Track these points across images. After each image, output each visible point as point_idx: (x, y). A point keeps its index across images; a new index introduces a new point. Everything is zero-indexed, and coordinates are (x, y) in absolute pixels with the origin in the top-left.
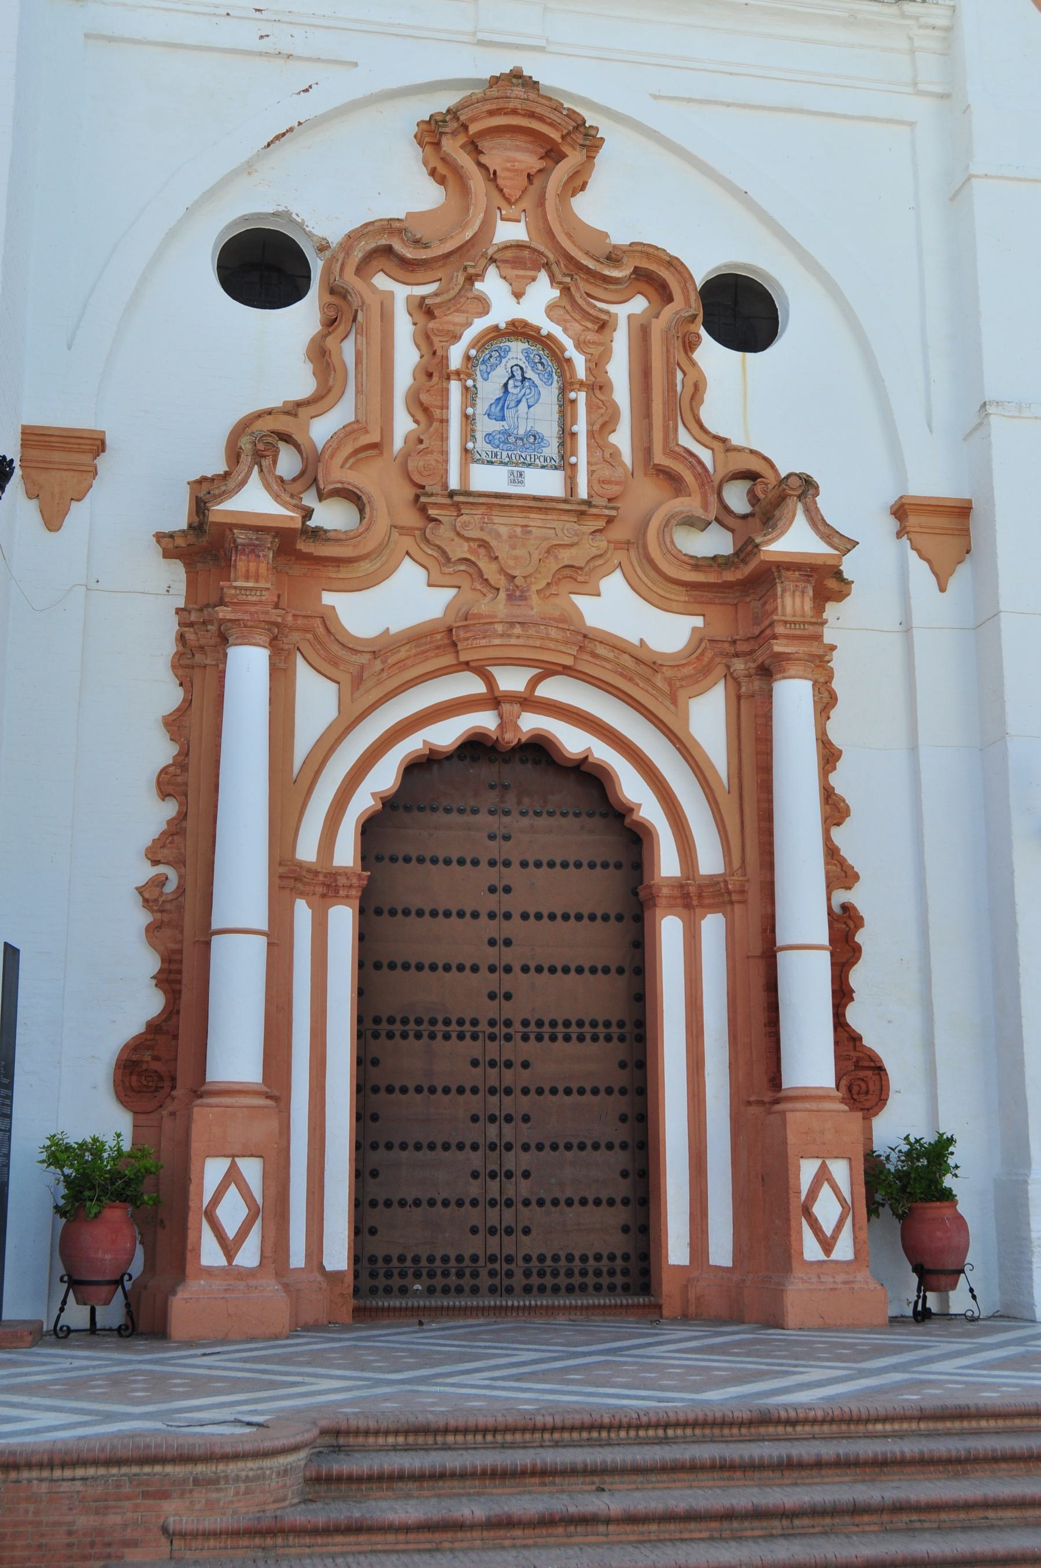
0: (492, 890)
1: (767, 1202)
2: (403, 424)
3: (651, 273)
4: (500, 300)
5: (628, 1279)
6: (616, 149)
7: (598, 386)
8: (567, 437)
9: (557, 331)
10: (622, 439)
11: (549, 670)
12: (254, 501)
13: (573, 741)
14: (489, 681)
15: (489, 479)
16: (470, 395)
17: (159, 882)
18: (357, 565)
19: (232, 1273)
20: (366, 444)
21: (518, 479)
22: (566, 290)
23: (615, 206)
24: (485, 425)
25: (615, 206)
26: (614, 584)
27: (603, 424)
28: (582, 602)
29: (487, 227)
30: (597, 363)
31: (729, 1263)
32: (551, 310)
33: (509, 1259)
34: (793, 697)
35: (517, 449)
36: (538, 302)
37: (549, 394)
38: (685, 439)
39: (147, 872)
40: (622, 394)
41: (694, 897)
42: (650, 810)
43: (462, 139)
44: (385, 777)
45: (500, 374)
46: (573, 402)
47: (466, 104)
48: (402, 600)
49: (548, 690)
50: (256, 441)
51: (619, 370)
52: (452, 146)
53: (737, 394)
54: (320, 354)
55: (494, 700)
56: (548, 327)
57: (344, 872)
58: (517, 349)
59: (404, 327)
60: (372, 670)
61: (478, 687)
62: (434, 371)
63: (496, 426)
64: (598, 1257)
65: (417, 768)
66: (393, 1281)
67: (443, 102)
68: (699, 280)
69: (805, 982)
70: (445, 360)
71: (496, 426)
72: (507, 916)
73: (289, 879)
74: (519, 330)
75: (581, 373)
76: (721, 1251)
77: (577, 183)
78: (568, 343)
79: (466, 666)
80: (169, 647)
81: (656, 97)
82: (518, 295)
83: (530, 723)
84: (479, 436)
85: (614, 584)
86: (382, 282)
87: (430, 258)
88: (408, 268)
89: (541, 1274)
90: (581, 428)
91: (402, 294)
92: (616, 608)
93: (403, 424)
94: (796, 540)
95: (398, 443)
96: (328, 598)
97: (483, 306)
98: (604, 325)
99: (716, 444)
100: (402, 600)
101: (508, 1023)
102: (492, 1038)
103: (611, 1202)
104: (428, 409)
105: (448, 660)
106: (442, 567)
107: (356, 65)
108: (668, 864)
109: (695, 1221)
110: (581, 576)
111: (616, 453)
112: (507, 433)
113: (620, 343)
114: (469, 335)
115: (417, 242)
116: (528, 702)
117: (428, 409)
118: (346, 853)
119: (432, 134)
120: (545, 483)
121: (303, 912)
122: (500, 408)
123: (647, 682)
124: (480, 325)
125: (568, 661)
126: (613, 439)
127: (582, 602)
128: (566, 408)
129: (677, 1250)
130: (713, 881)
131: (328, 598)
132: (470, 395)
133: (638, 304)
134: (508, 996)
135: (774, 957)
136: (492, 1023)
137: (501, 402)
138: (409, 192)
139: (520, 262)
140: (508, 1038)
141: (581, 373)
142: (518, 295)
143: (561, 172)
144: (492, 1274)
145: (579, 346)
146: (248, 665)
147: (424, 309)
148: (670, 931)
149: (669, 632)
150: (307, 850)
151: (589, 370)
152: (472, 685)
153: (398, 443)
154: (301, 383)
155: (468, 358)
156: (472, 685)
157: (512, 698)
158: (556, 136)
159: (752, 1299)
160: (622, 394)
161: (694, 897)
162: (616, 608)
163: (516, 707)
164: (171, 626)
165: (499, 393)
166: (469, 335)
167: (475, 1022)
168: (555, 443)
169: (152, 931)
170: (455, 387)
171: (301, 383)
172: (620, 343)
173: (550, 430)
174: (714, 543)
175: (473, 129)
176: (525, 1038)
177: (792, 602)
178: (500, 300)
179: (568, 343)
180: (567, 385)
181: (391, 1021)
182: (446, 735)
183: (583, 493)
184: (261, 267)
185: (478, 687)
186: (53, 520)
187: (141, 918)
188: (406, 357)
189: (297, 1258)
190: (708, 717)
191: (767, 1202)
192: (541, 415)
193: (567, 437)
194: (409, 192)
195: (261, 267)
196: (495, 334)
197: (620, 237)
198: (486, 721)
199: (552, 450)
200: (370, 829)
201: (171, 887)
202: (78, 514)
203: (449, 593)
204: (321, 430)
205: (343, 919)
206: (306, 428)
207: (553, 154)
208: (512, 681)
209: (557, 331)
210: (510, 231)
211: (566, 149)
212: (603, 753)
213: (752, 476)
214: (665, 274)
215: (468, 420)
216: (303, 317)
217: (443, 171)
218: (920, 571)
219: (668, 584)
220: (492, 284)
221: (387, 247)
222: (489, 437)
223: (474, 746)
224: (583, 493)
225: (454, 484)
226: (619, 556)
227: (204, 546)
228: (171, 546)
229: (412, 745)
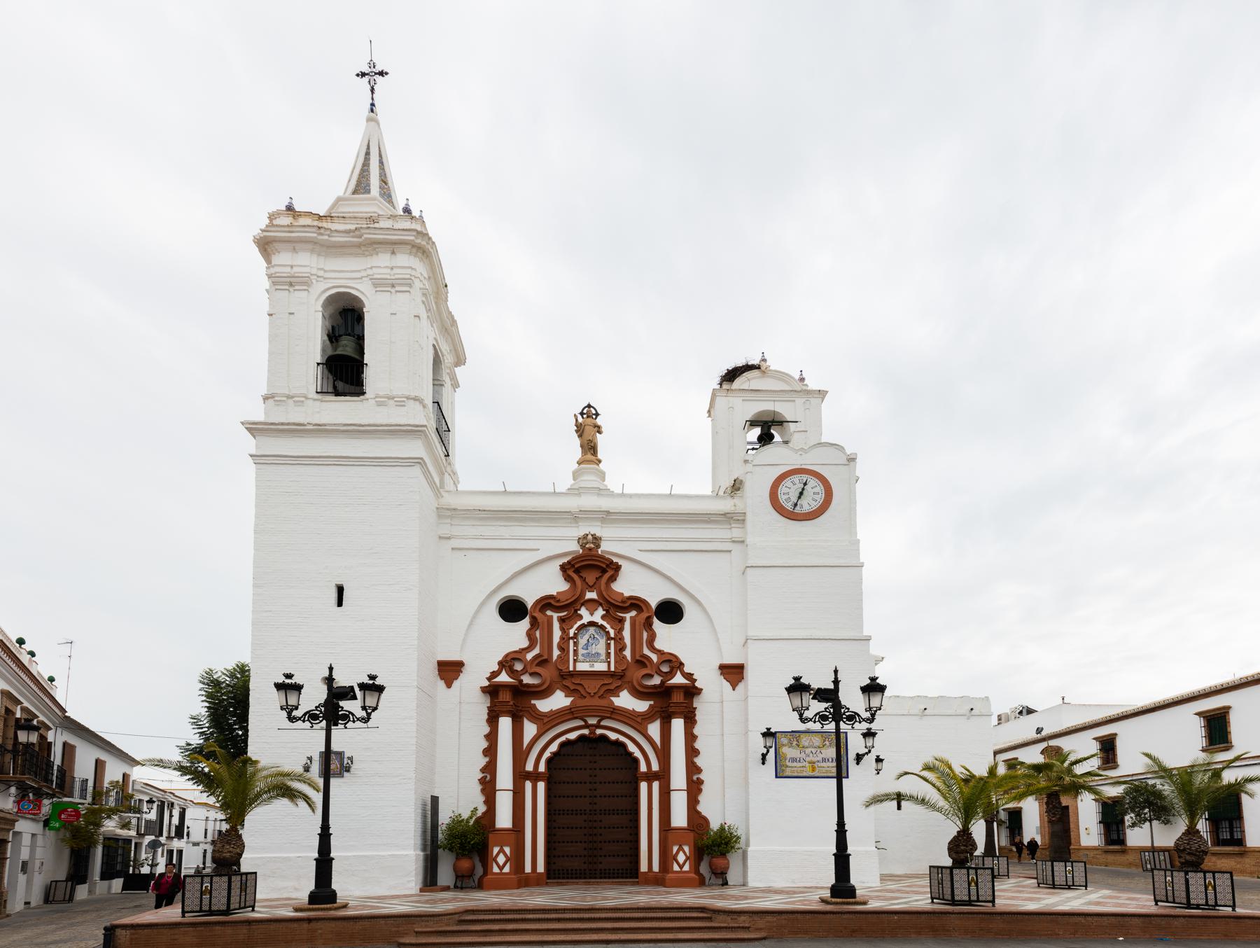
1: (667, 858)
2: (556, 653)
3: (636, 604)
4: (586, 616)
5: (628, 871)
6: (626, 567)
8: (608, 654)
9: (605, 623)
10: (627, 653)
11: (603, 718)
12: (504, 678)
13: (613, 736)
15: (582, 667)
16: (576, 644)
18: (544, 693)
19: (501, 873)
20: (542, 661)
22: (607, 611)
23: (626, 585)
24: (581, 651)
25: (626, 585)
27: (623, 648)
28: (613, 699)
32: (603, 617)
34: (678, 725)
35: (593, 657)
37: (602, 642)
39: (480, 775)
40: (628, 640)
41: (650, 777)
42: (638, 754)
44: (554, 747)
45: (586, 637)
47: (573, 559)
48: (558, 701)
49: (603, 723)
50: (507, 663)
51: (627, 634)
52: (571, 573)
53: (667, 637)
54: (530, 635)
55: (587, 726)
56: (601, 622)
58: (592, 630)
59: (556, 625)
60: (547, 721)
61: (582, 723)
62: (565, 639)
65: (562, 745)
66: (557, 873)
67: (565, 560)
68: (654, 604)
69: (679, 803)
73: (520, 776)
74: (592, 624)
75: (612, 635)
76: (656, 868)
77: (613, 578)
80: (486, 717)
83: (599, 732)
86: (549, 613)
87: (567, 606)
90: (612, 651)
91: (555, 616)
92: (625, 700)
93: (556, 653)
94: (678, 679)
95: (555, 657)
97: (581, 617)
98: (622, 621)
100: (558, 701)
104: (563, 649)
106: (569, 692)
107: (340, 604)
108: (643, 768)
109: (648, 857)
110: (616, 692)
111: (624, 657)
113: (627, 625)
114: (576, 626)
116: (598, 726)
119: (563, 568)
120: (601, 667)
122: (586, 646)
123: (638, 721)
124: (579, 623)
127: (613, 699)
128: (608, 646)
130: (656, 773)
132: (576, 644)
133: (633, 613)
138: (556, 585)
141: (612, 635)
143: (607, 575)
146: (505, 723)
148: (643, 786)
149: (642, 706)
153: (555, 657)
154: (525, 643)
159: (659, 880)
160: (628, 640)
162: (625, 700)
169: (483, 791)
170: (571, 642)
171: (525, 643)
172: (627, 625)
173: (602, 651)
174: (656, 680)
178: (586, 616)
180: (609, 638)
182: (573, 736)
183: (612, 669)
184: (511, 610)
185: (582, 723)
187: (479, 787)
188: (557, 634)
189: (528, 869)
190: (654, 729)
191: (667, 858)
192: (600, 647)
193: (608, 654)
194: (556, 585)
195: (511, 610)
196: (583, 626)
197: (627, 594)
198: (586, 732)
199: (603, 657)
202: (456, 684)
204: (529, 656)
205: (541, 786)
207: (604, 571)
208: (593, 721)
209: (605, 623)
212: (622, 739)
213: (669, 661)
216: (525, 624)
217: (568, 578)
218: (727, 685)
219: (639, 694)
221: (547, 603)
223: (581, 737)
227: (492, 690)
229: (563, 739)
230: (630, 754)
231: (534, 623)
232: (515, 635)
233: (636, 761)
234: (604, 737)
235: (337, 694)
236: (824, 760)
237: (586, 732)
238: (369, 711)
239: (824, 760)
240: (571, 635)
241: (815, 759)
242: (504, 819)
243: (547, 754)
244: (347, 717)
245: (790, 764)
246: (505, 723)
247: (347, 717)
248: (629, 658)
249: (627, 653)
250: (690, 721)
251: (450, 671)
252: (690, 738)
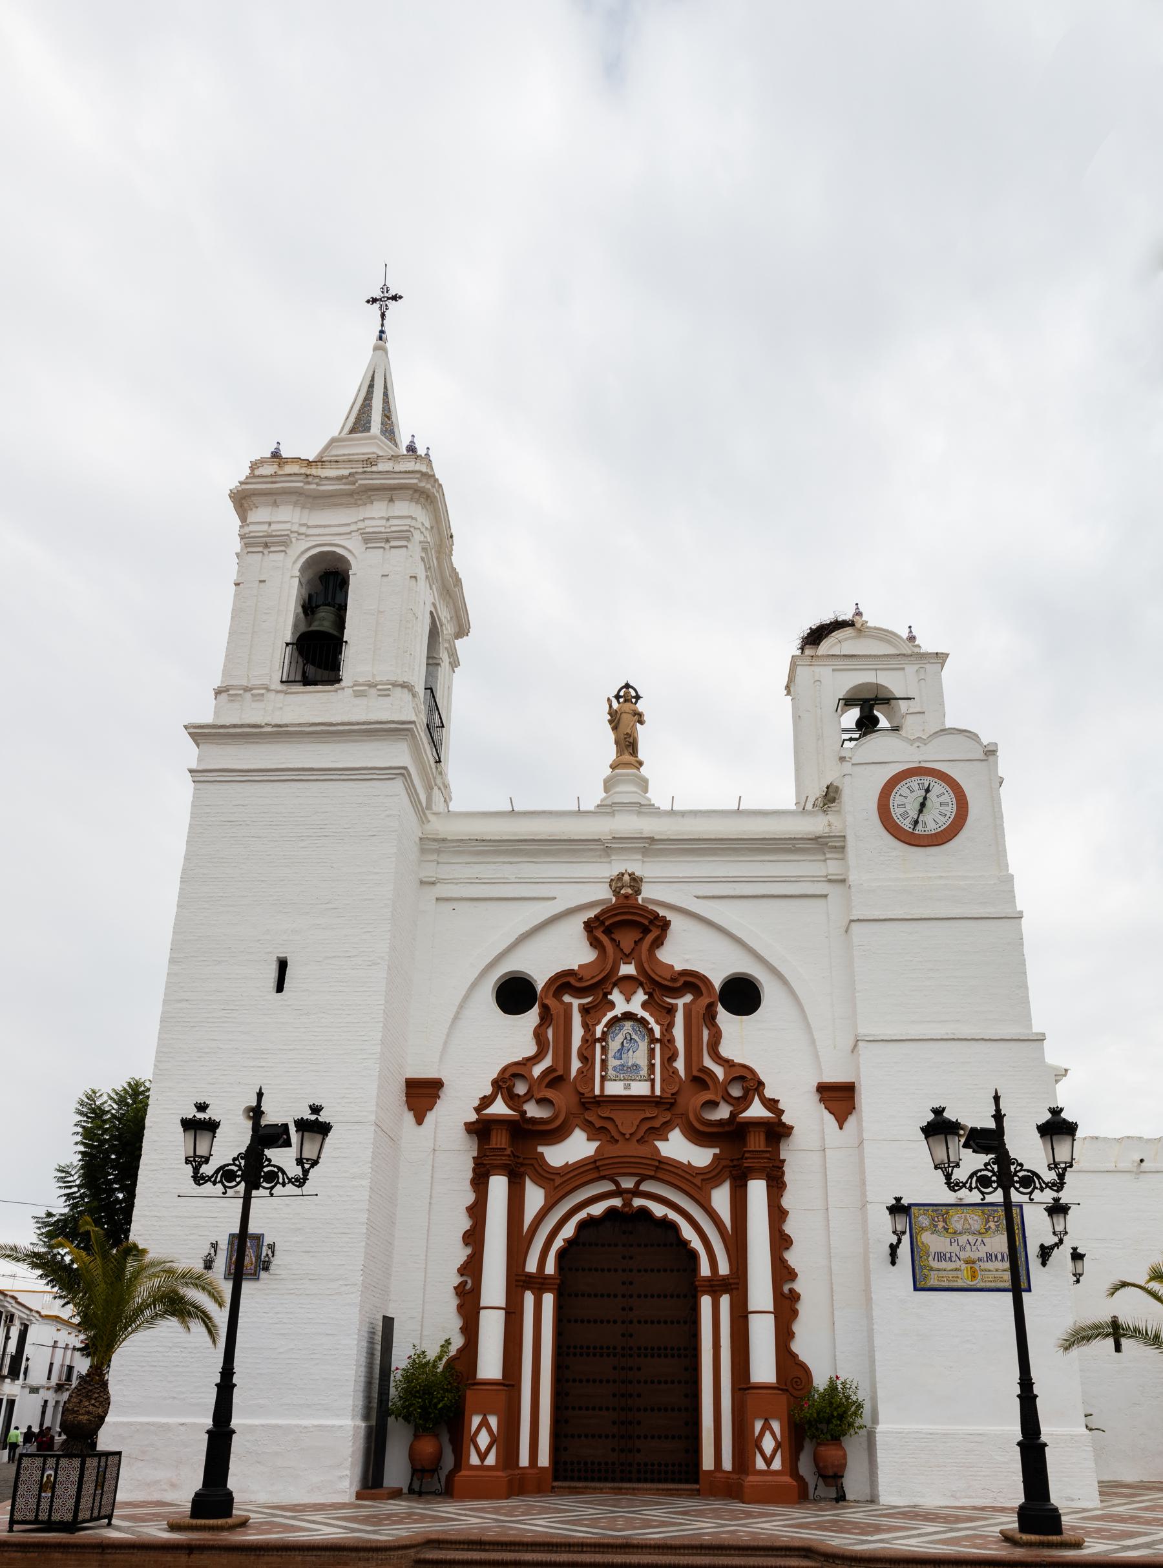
0: (624, 1283)
2: (576, 1064)
3: (692, 982)
6: (678, 924)
7: (667, 1041)
8: (652, 1067)
9: (646, 1015)
10: (680, 1065)
11: (643, 1178)
12: (499, 1108)
13: (659, 1210)
14: (617, 1184)
15: (614, 1088)
16: (604, 1050)
17: (464, 1283)
18: (556, 1133)
20: (555, 1078)
21: (628, 1087)
23: (682, 951)
24: (612, 1063)
25: (682, 951)
26: (676, 1135)
28: (659, 1144)
29: (615, 968)
30: (668, 1028)
31: (712, 1468)
32: (644, 1005)
33: (630, 1465)
34: (757, 1190)
35: (628, 1072)
36: (636, 1004)
37: (643, 1046)
38: (708, 1062)
40: (680, 1043)
42: (696, 1244)
43: (602, 929)
44: (568, 1231)
45: (620, 1038)
46: (653, 1049)
47: (603, 912)
48: (576, 1148)
49: (645, 1187)
53: (740, 1038)
57: (549, 1277)
58: (628, 1026)
60: (560, 1183)
61: (611, 1187)
62: (589, 1041)
63: (618, 1062)
64: (666, 1465)
67: (592, 914)
68: (717, 984)
69: (762, 1331)
70: (594, 1033)
71: (618, 1062)
72: (631, 1296)
74: (628, 1016)
75: (658, 1035)
77: (659, 942)
78: (651, 1020)
79: (603, 1178)
81: (697, 897)
82: (628, 1000)
83: (638, 1202)
84: (610, 1068)
85: (676, 1135)
86: (567, 999)
88: (579, 992)
89: (646, 1472)
90: (657, 1061)
91: (576, 1003)
92: (677, 1147)
93: (576, 1064)
94: (757, 1110)
95: (574, 1073)
96: (540, 1149)
97: (612, 1005)
98: (671, 1010)
99: (726, 1065)
100: (576, 1148)
101: (631, 1348)
102: (623, 1356)
103: (680, 1437)
104: (586, 1059)
105: (596, 1175)
106: (593, 1132)
108: (705, 1270)
109: (715, 1448)
110: (661, 1133)
111: (675, 1072)
112: (623, 1066)
114: (605, 1020)
115: (581, 979)
116: (636, 1193)
117: (586, 1059)
118: (550, 1268)
120: (640, 1089)
121: (529, 1298)
122: (620, 1054)
123: (696, 1184)
124: (610, 1015)
125: (652, 1173)
126: (675, 1064)
127: (659, 1144)
128: (652, 1052)
129: (708, 1463)
130: (725, 1278)
131: (540, 1149)
132: (604, 1050)
133: (688, 998)
134: (631, 1336)
135: (746, 1318)
136: (623, 1348)
137: (620, 1051)
139: (628, 985)
140: (631, 1356)
141: (658, 1035)
142: (628, 1000)
143: (650, 937)
144: (630, 1472)
145: (657, 1022)
146: (498, 1185)
147: (585, 1010)
149: (700, 1157)
150: (531, 1266)
151: (662, 1033)
152: (609, 1187)
153: (574, 1073)
154: (531, 1050)
155: (603, 1033)
156: (609, 1187)
157: (627, 1191)
158: (646, 922)
159: (733, 1487)
160: (680, 1043)
161: (717, 1286)
162: (677, 1147)
163: (630, 1195)
164: (470, 1165)
165: (619, 1047)
166: (605, 1020)
167: (615, 1348)
168: (646, 1069)
170: (598, 1046)
171: (531, 1050)
173: (643, 1063)
174: (723, 1112)
175: (607, 923)
176: (639, 1356)
177: (756, 1142)
178: (620, 1004)
179: (651, 1020)
180: (653, 1040)
181: (575, 1347)
182: (597, 1209)
183: (658, 1092)
184: (514, 994)
185: (611, 1187)
186: (420, 1121)
188: (578, 1033)
189: (524, 1461)
190: (721, 1199)
192: (639, 1056)
193: (652, 1067)
196: (615, 1020)
198: (617, 1202)
199: (644, 1072)
200: (561, 1255)
201: (469, 1286)
202: (430, 1117)
203: (596, 1144)
205: (548, 1299)
206: (531, 1071)
207: (646, 931)
208: (628, 1184)
209: (646, 1015)
210: (628, 969)
211: (651, 927)
212: (673, 1215)
213: (742, 1078)
214: (701, 985)
215: (604, 1062)
216: (532, 1017)
217: (595, 943)
218: (830, 1119)
219: (699, 1135)
220: (616, 996)
221: (564, 983)
222: (614, 1068)
223: (611, 1212)
224: (658, 1092)
225: (597, 1092)
226: (679, 1121)
228: (470, 1128)
229: (582, 1215)
230: (685, 1243)
231: (546, 1016)
232: (516, 1037)
233: (694, 1256)
234: (645, 1212)
235: (267, 1136)
236: (989, 1257)
237: (617, 1202)
238: (307, 1164)
239: (989, 1257)
240: (598, 1035)
241: (975, 1256)
242: (490, 1366)
243: (558, 1243)
244: (274, 1177)
245: (935, 1264)
246: (498, 1185)
247: (274, 1177)
248: (682, 1073)
249: (680, 1065)
250: (776, 1186)
251: (422, 1094)
252: (777, 1215)
